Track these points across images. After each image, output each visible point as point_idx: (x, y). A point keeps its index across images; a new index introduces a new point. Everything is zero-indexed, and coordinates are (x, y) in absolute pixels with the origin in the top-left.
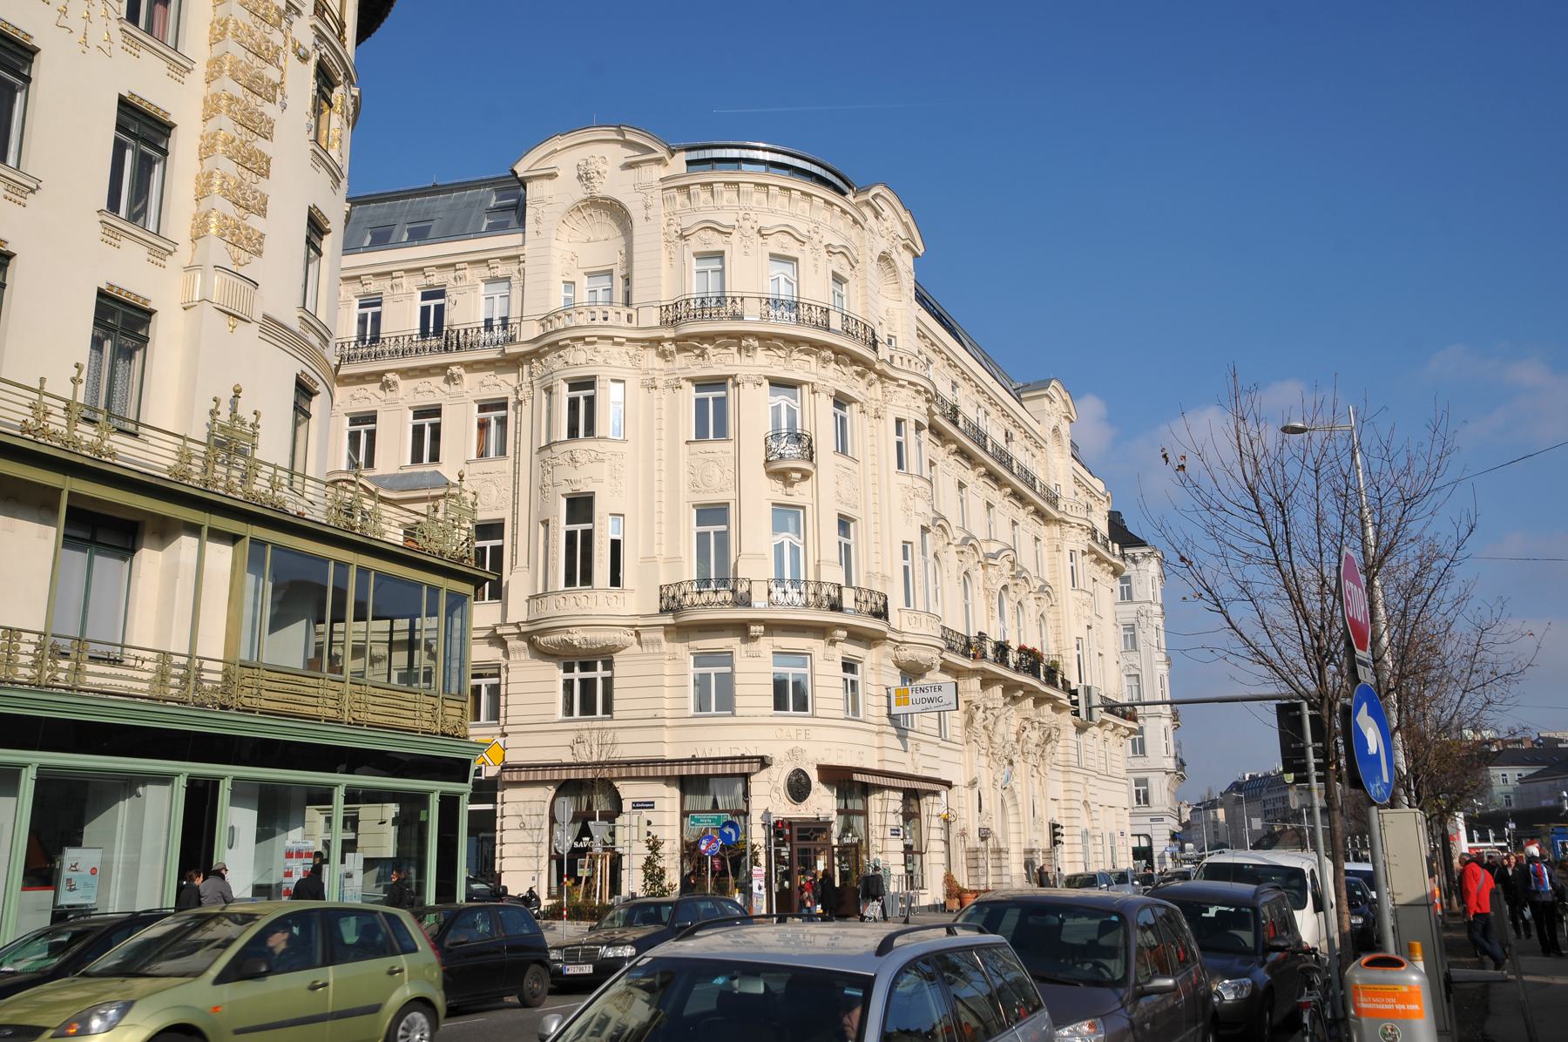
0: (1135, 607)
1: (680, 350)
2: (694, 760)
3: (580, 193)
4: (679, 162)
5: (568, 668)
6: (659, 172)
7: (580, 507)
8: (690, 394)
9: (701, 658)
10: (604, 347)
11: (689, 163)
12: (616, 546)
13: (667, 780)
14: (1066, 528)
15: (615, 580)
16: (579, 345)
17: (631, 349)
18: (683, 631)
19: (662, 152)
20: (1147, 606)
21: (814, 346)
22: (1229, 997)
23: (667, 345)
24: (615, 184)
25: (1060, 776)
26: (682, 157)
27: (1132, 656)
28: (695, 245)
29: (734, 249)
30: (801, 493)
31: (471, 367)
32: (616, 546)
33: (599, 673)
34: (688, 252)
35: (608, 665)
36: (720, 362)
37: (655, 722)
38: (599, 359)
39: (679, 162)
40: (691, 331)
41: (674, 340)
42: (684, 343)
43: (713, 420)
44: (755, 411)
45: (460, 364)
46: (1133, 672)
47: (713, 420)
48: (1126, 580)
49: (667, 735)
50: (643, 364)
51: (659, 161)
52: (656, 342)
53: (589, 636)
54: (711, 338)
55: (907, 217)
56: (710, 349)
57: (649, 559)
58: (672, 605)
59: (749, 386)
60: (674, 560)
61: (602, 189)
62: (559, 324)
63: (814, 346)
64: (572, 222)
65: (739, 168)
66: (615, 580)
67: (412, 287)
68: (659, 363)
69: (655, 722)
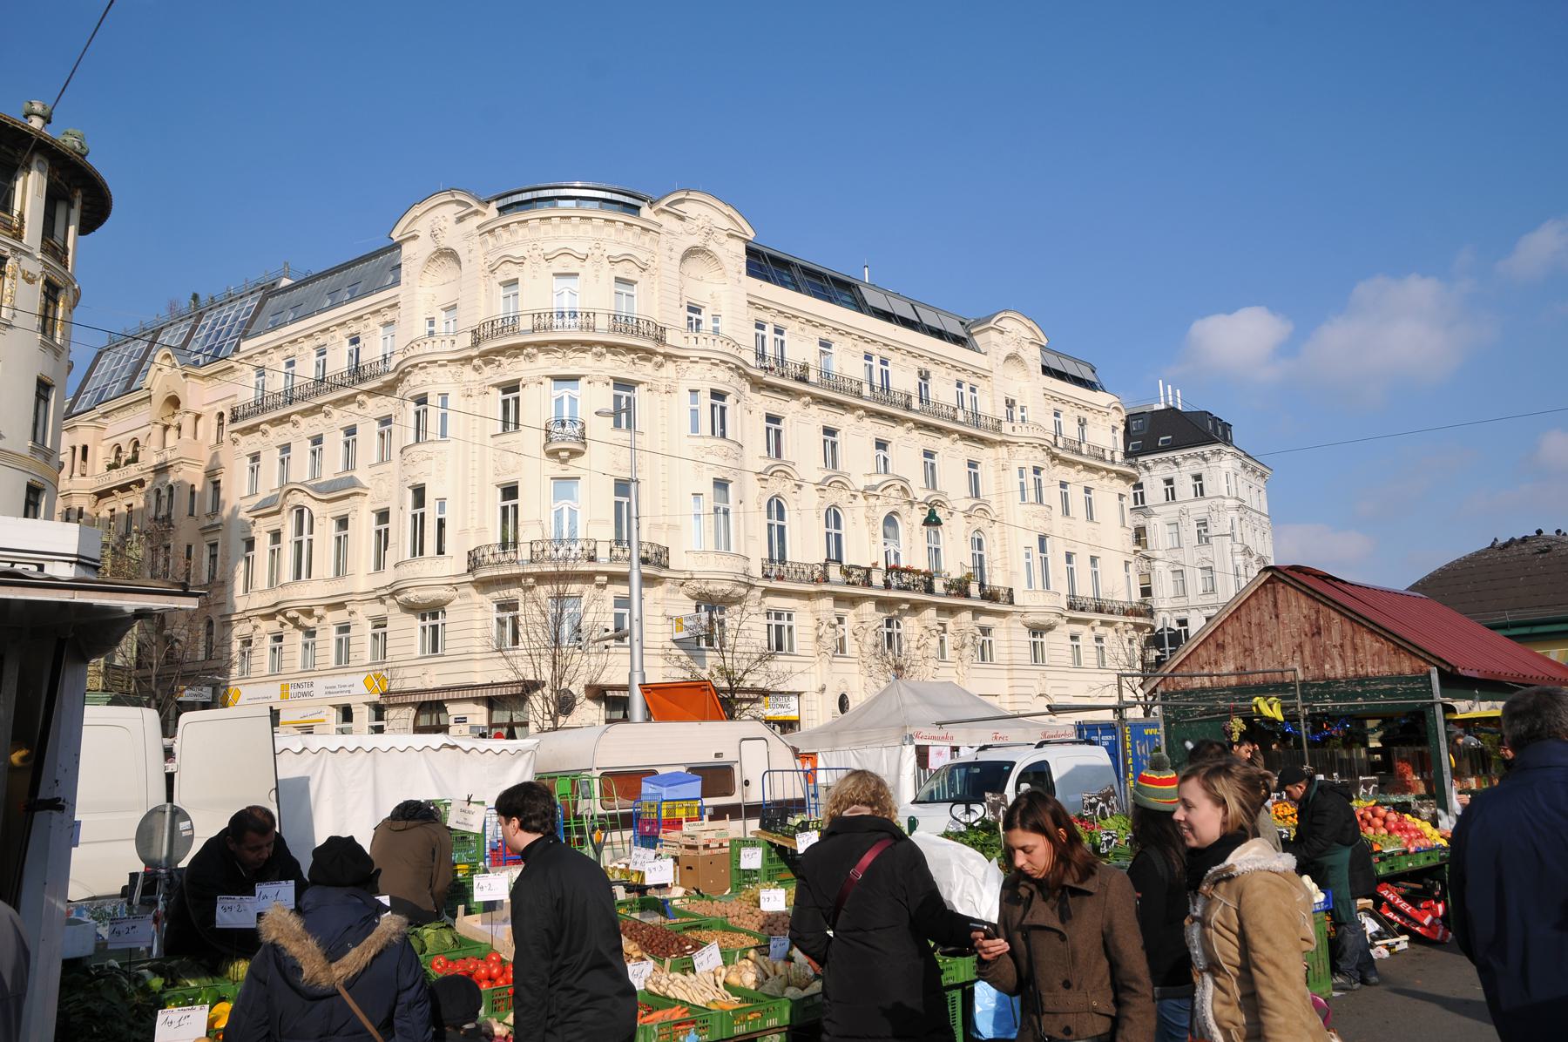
0: (1205, 503)
1: (486, 364)
2: (493, 685)
3: (431, 248)
4: (492, 210)
5: (424, 619)
6: (479, 220)
7: (419, 494)
8: (498, 396)
9: (502, 607)
10: (432, 369)
11: (500, 209)
12: (441, 523)
13: (476, 700)
14: (1014, 448)
15: (440, 552)
16: (416, 371)
17: (453, 368)
18: (485, 585)
19: (476, 206)
20: (1220, 501)
21: (585, 346)
22: (1381, 871)
23: (475, 362)
24: (453, 236)
25: (1005, 674)
26: (494, 205)
27: (1204, 549)
28: (501, 276)
29: (524, 275)
30: (575, 467)
31: (371, 393)
32: (441, 523)
33: (784, 622)
34: (495, 283)
35: (789, 617)
36: (510, 369)
37: (467, 657)
38: (429, 380)
39: (492, 210)
40: (491, 347)
41: (480, 356)
42: (488, 357)
43: (510, 419)
44: (537, 404)
45: (364, 392)
46: (1178, 568)
47: (510, 419)
48: (1140, 486)
49: (477, 666)
50: (465, 378)
51: (476, 213)
52: (469, 360)
53: (420, 594)
54: (500, 351)
55: (729, 210)
56: (503, 359)
57: (464, 531)
58: (474, 561)
59: (532, 386)
60: (482, 530)
61: (445, 243)
62: (412, 353)
63: (585, 346)
64: (434, 265)
65: (555, 205)
66: (440, 552)
67: (341, 336)
68: (474, 375)
69: (467, 657)
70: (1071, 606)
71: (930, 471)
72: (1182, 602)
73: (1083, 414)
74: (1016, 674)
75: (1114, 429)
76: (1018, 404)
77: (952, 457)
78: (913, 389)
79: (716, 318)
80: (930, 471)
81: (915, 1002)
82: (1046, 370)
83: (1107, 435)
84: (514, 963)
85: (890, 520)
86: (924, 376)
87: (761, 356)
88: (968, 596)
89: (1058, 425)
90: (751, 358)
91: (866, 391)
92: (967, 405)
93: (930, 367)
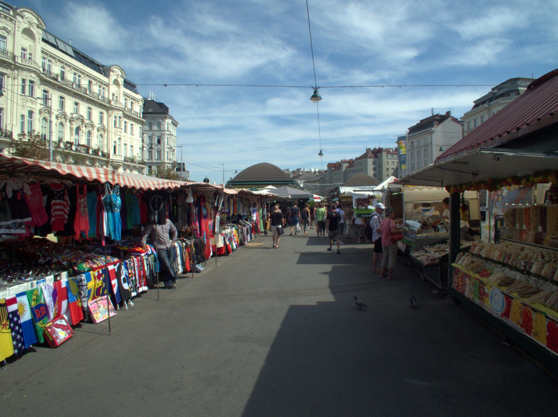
27: (159, 146)
70: (125, 160)
71: (90, 114)
72: (150, 161)
73: (133, 101)
74: (12, 164)
75: (141, 107)
76: (116, 95)
77: (96, 111)
78: (86, 87)
79: (30, 54)
80: (90, 114)
81: (307, 239)
82: (44, 40)
83: (138, 108)
84: (459, 220)
85: (78, 129)
86: (90, 83)
87: (44, 70)
88: (98, 155)
89: (126, 103)
90: (41, 70)
91: (59, 79)
92: (77, 82)
93: (92, 80)
